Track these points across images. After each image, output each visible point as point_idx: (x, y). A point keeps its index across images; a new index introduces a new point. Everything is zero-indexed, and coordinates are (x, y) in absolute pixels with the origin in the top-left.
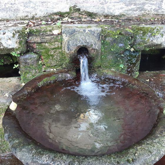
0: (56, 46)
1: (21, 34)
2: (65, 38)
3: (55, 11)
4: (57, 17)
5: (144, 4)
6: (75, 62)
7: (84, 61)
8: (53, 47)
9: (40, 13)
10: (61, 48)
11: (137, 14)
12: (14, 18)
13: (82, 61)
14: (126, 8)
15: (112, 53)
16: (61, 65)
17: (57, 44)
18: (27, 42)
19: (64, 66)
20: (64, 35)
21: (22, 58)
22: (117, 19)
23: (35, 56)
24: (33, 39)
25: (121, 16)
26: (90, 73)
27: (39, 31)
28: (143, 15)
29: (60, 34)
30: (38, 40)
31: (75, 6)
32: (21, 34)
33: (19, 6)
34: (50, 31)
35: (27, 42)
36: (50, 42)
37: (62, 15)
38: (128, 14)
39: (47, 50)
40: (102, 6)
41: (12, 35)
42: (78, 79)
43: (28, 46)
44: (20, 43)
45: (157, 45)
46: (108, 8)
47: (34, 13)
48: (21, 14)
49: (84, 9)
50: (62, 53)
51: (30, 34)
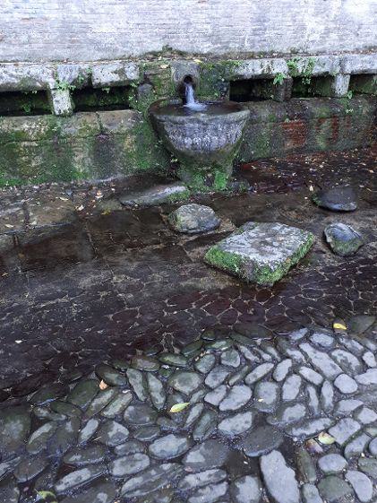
2: (173, 71)
3: (150, 50)
4: (151, 56)
7: (191, 91)
11: (223, 52)
12: (112, 57)
14: (213, 47)
17: (166, 76)
21: (140, 88)
24: (147, 72)
25: (209, 54)
26: (195, 99)
29: (169, 67)
42: (185, 101)
48: (119, 54)
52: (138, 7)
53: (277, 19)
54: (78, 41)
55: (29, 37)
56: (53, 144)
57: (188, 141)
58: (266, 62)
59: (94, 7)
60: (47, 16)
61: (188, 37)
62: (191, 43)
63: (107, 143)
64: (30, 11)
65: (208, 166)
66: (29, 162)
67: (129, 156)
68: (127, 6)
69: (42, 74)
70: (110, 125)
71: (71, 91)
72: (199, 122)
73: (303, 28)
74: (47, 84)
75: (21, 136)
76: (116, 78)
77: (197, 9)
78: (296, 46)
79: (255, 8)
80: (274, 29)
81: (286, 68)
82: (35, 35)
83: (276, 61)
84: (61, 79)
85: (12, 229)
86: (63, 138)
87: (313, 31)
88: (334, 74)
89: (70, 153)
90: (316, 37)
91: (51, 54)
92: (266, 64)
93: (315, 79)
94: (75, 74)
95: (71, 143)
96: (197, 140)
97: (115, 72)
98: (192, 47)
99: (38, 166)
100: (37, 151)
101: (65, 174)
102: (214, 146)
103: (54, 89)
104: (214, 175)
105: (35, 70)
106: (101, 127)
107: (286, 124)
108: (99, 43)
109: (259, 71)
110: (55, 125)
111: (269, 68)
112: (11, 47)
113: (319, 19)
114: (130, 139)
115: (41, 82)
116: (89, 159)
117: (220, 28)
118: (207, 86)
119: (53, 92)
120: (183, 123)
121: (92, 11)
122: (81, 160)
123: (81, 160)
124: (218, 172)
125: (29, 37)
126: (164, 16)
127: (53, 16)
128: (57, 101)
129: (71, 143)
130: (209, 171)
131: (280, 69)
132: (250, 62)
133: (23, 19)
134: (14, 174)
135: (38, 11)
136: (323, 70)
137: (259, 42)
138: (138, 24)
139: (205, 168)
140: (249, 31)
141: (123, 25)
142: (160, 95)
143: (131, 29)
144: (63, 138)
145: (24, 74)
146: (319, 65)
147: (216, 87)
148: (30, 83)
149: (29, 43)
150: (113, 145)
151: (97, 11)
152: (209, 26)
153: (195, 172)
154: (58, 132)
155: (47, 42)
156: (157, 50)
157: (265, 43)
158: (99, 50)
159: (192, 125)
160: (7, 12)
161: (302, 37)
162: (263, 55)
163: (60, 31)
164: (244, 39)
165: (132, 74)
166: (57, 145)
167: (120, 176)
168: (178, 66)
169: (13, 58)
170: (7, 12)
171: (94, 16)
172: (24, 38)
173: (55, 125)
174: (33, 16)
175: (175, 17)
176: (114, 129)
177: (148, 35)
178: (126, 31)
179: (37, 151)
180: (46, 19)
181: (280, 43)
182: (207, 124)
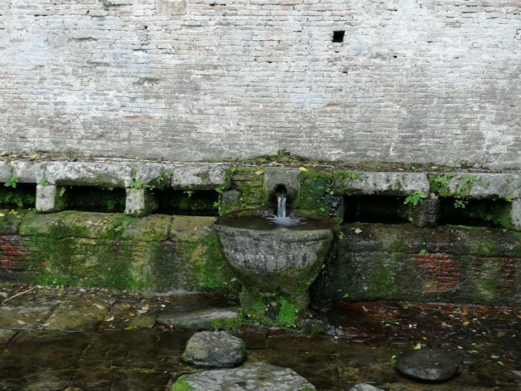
0: (258, 185)
1: (228, 172)
2: (266, 178)
3: (262, 153)
4: (264, 160)
5: (366, 150)
6: (273, 200)
7: (281, 200)
8: (255, 185)
9: (246, 154)
10: (262, 186)
11: (358, 160)
12: (216, 159)
13: (279, 199)
15: (311, 195)
16: (260, 203)
17: (258, 183)
18: (232, 180)
19: (263, 204)
20: (266, 175)
21: (225, 194)
22: (334, 165)
23: (237, 193)
24: (236, 177)
25: (338, 162)
27: (243, 171)
28: (366, 163)
30: (242, 178)
31: (284, 150)
32: (228, 172)
33: (224, 147)
34: (254, 171)
35: (232, 180)
36: (252, 180)
37: (269, 159)
38: (347, 161)
39: (249, 187)
40: (315, 151)
41: (220, 173)
43: (232, 184)
44: (226, 180)
45: (357, 190)
46: (322, 152)
47: (238, 155)
48: (224, 156)
49: (295, 153)
50: (262, 192)
51: (235, 173)
52: (253, 109)
53: (439, 125)
54: (180, 141)
55: (130, 134)
56: (113, 245)
57: (239, 256)
58: (394, 176)
59: (202, 108)
60: (152, 115)
61: (311, 142)
62: (315, 148)
63: (173, 251)
64: (135, 110)
65: (270, 291)
66: (83, 261)
67: (197, 269)
68: (239, 108)
69: (119, 171)
70: (179, 231)
71: (147, 192)
72: (249, 236)
73: (480, 137)
74: (122, 181)
75: (79, 233)
76: (198, 181)
77: (326, 112)
78: (469, 159)
79: (404, 112)
80: (434, 137)
81: (425, 185)
82: (135, 132)
83: (410, 175)
84: (137, 178)
85: (22, 326)
86: (124, 239)
87: (495, 142)
88: (508, 199)
89: (129, 256)
90: (502, 149)
91: (149, 152)
92: (394, 178)
93: (474, 203)
94: (155, 174)
95: (131, 246)
96: (250, 257)
97: (198, 175)
98: (317, 153)
99: (91, 268)
100: (94, 250)
101: (119, 279)
102: (271, 266)
103: (129, 187)
104: (280, 305)
105: (112, 168)
106: (169, 233)
107: (423, 257)
108: (203, 143)
109: (385, 187)
110: (121, 224)
111: (399, 184)
112: (110, 143)
113: (504, 127)
114: (200, 250)
115: (116, 179)
116: (149, 267)
117: (355, 134)
118: (309, 198)
119: (128, 190)
120: (233, 235)
121: (200, 112)
122: (140, 267)
123: (140, 267)
124: (284, 302)
125: (130, 134)
126: (283, 119)
127: (157, 115)
128: (130, 200)
129: (131, 246)
130: (273, 299)
131: (416, 185)
132: (371, 175)
133: (127, 117)
134: (65, 271)
135: (143, 110)
136: (487, 192)
137: (410, 151)
138: (251, 126)
139: (268, 294)
140: (396, 137)
141: (233, 125)
142: (248, 204)
143: (242, 131)
144: (124, 239)
145: (102, 170)
146: (481, 185)
147: (321, 200)
148: (105, 180)
149: (128, 139)
150: (179, 255)
151: (205, 112)
152: (340, 131)
153: (256, 297)
154: (120, 233)
155: (147, 140)
156: (270, 154)
157: (421, 153)
158: (202, 150)
159: (242, 238)
160: (113, 110)
161: (479, 148)
162: (394, 167)
163: (163, 130)
164: (389, 147)
165: (217, 178)
166: (116, 246)
167: (181, 292)
168: (273, 173)
169: (110, 154)
170: (113, 110)
171: (201, 117)
172: (124, 135)
173: (121, 224)
174: (138, 114)
175: (297, 120)
176: (183, 236)
177: (261, 138)
178: (235, 133)
179: (94, 250)
180: (151, 118)
181: (442, 154)
182: (259, 240)
